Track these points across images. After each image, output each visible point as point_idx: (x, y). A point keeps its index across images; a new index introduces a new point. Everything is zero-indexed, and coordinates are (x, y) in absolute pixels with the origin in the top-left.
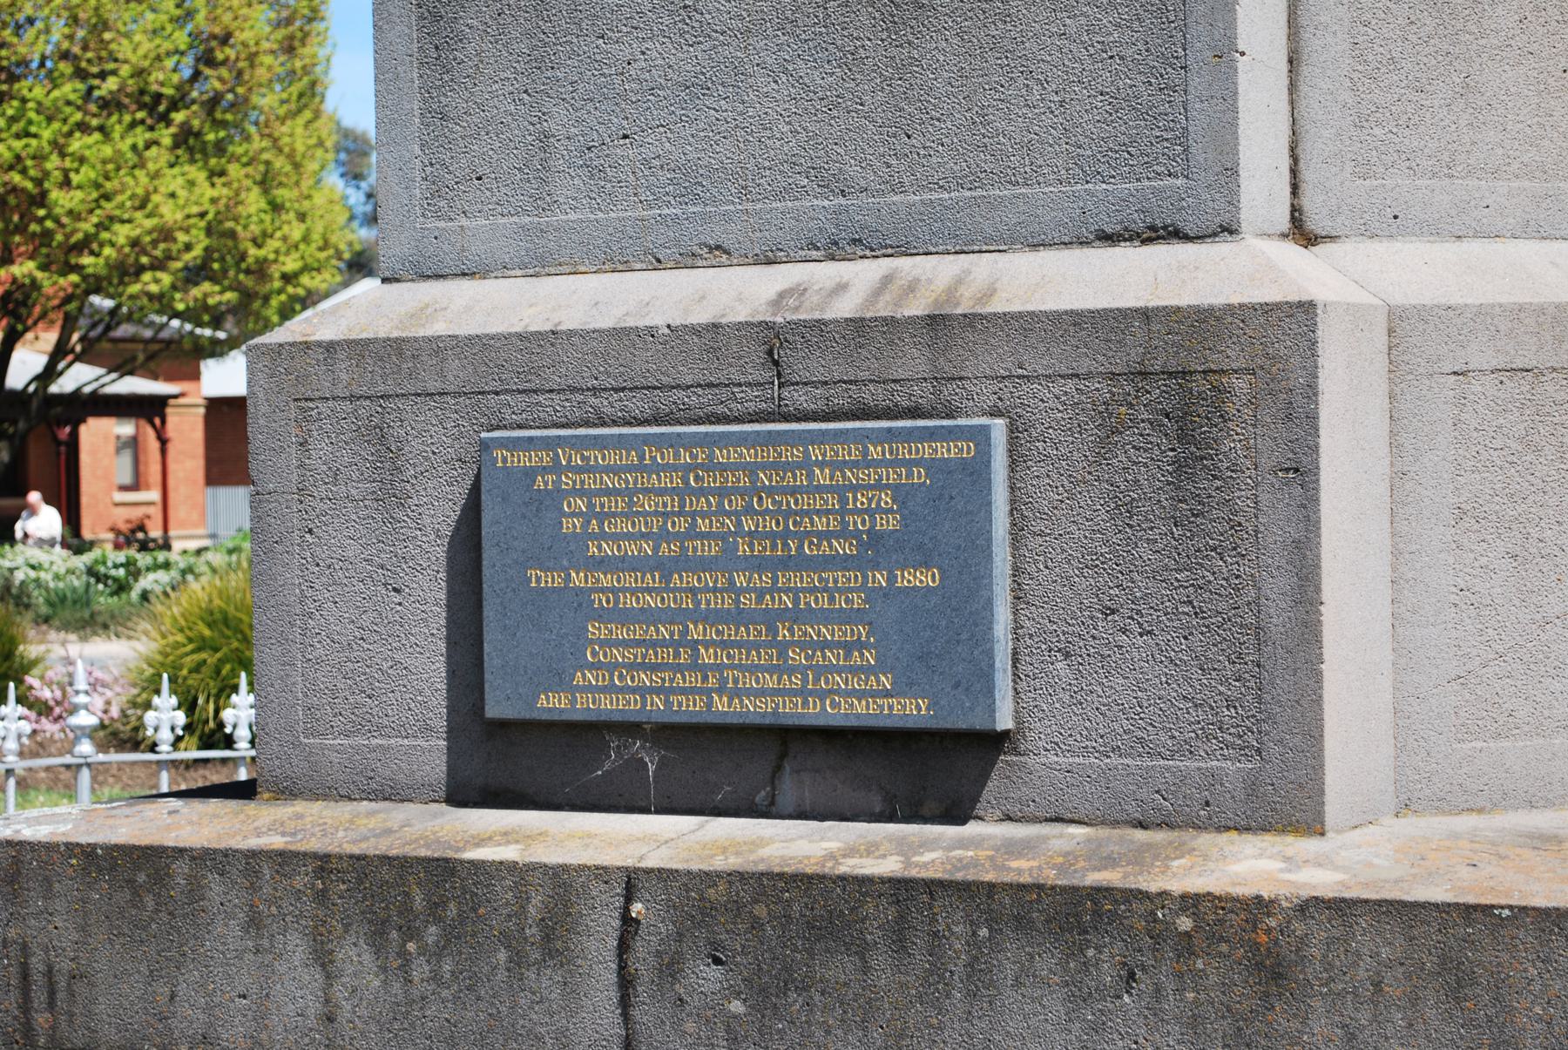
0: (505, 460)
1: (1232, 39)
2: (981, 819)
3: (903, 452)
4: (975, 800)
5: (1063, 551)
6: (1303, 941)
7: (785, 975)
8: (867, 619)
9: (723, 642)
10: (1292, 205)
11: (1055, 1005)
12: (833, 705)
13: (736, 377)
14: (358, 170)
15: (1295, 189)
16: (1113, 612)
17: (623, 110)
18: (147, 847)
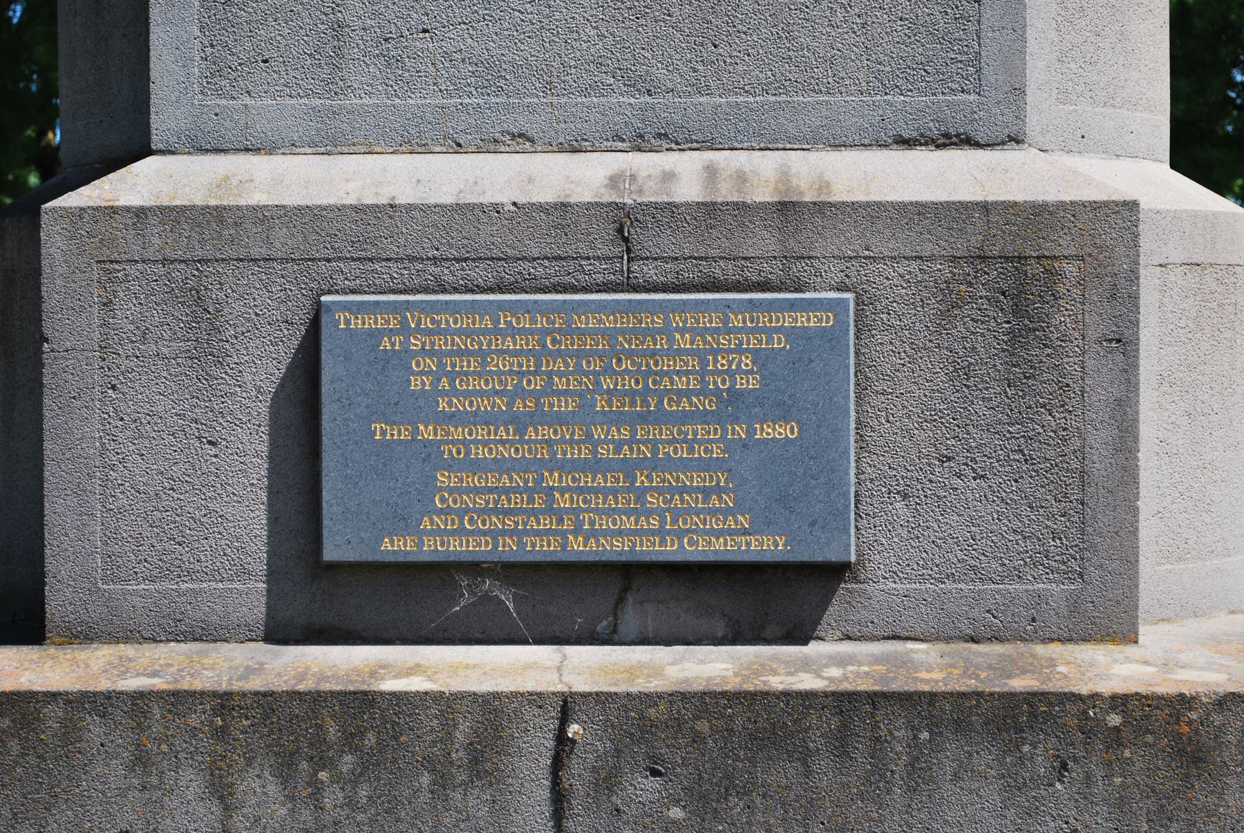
0: (348, 322)
2: (822, 639)
3: (764, 320)
4: (817, 622)
5: (904, 407)
6: (1221, 729)
7: (726, 782)
8: (725, 467)
9: (579, 488)
11: (992, 795)
12: (691, 542)
13: (584, 249)
16: (949, 459)
18: (12, 693)
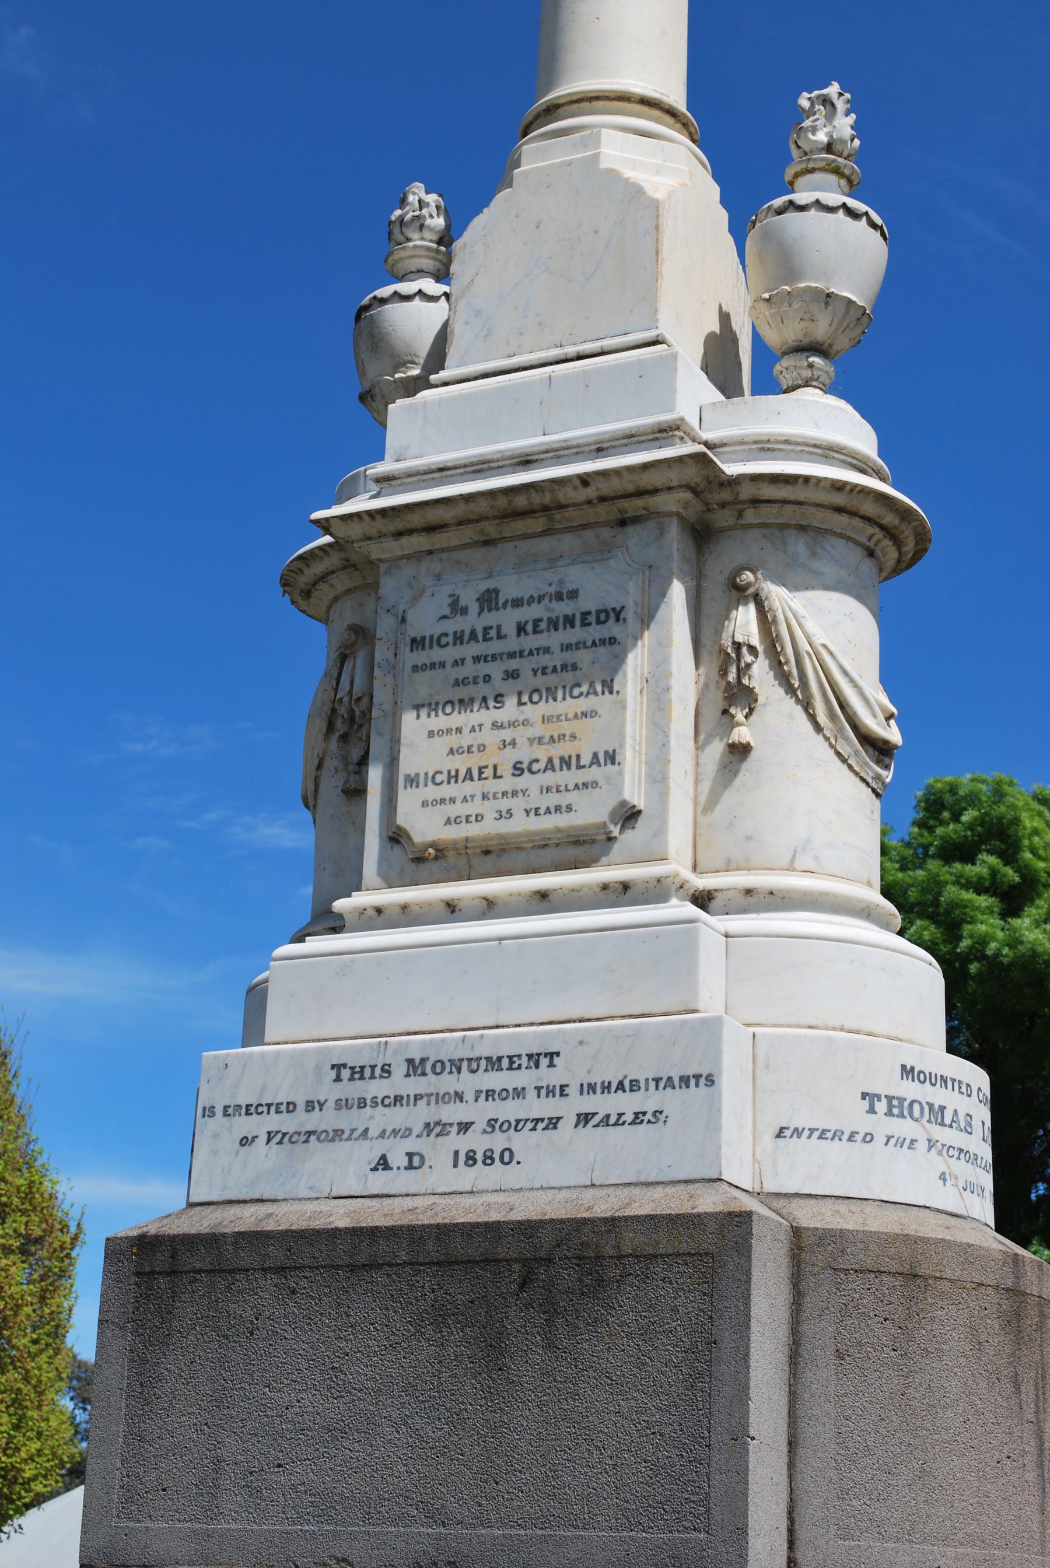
1: (745, 1426)
10: (789, 1558)
14: (86, 1395)
15: (791, 1544)
17: (279, 1445)
